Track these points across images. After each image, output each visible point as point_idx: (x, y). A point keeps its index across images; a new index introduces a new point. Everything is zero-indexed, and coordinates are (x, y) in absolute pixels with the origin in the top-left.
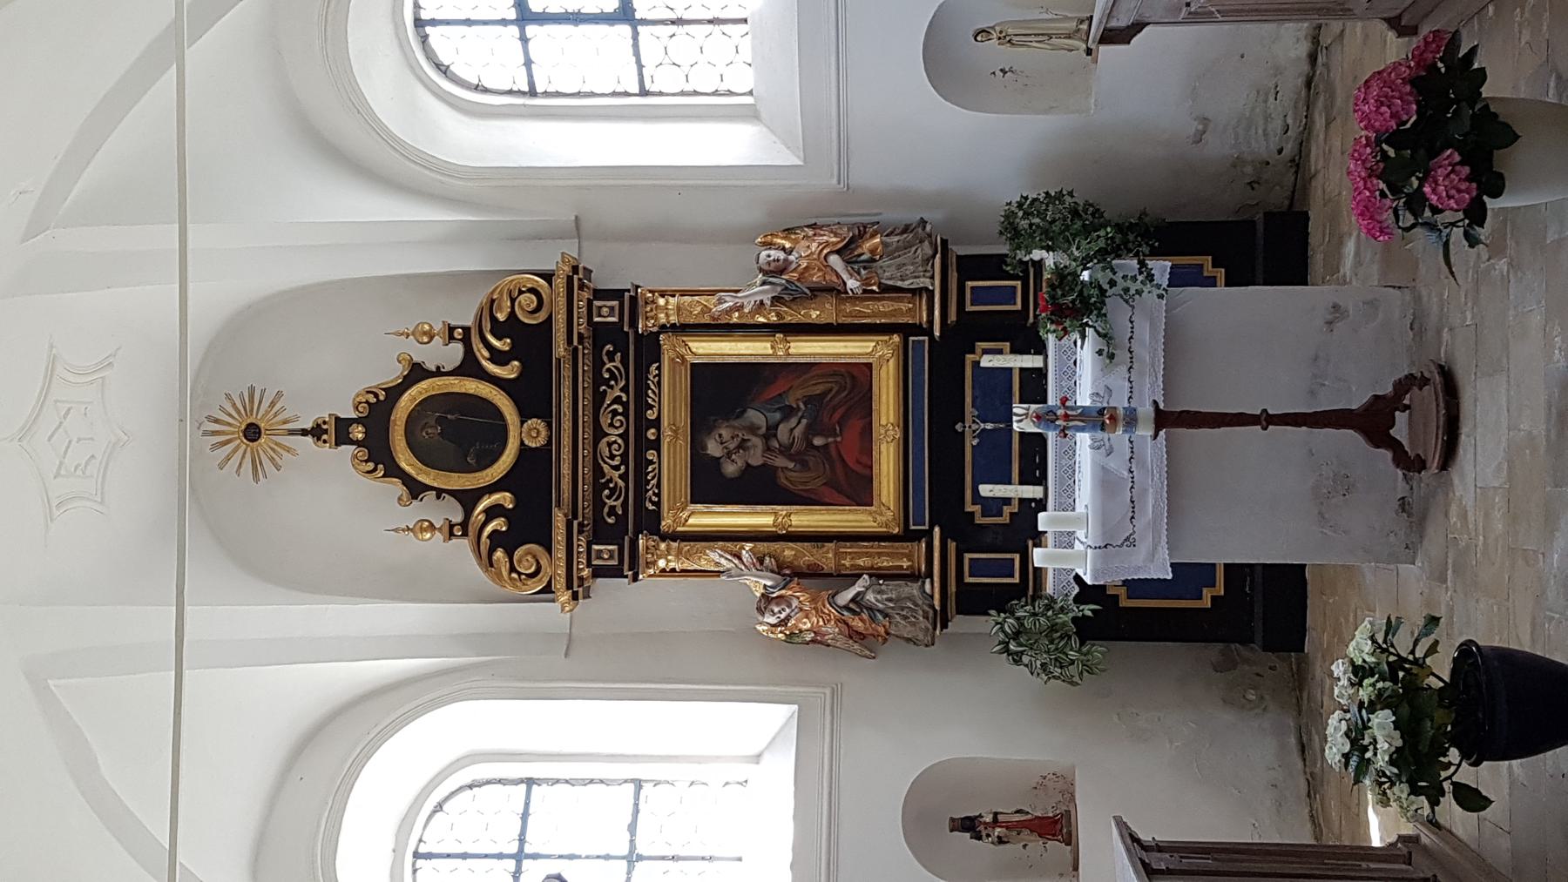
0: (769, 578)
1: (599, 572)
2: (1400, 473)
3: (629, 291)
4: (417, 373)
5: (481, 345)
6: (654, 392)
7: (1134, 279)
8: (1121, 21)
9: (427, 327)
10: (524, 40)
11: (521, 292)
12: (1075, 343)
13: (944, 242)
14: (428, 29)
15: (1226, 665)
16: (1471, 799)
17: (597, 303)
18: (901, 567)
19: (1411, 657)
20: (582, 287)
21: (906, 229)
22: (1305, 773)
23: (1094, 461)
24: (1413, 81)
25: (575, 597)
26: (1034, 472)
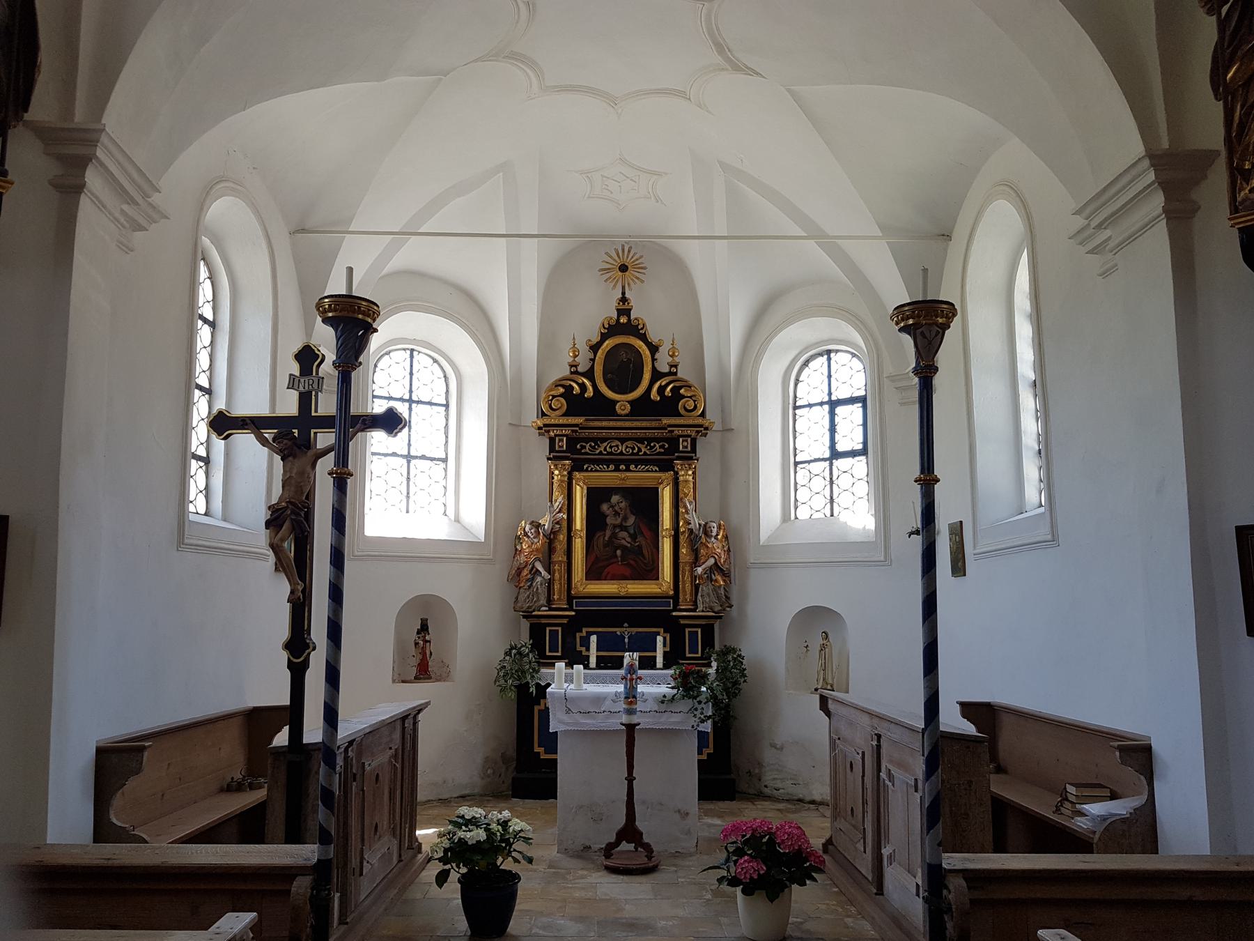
0: (548, 528)
1: (552, 440)
2: (603, 846)
3: (696, 456)
4: (654, 349)
5: (668, 381)
6: (644, 468)
7: (702, 713)
8: (831, 706)
9: (677, 354)
10: (821, 404)
11: (695, 401)
12: (669, 684)
13: (720, 617)
14: (826, 357)
15: (505, 759)
16: (442, 878)
17: (689, 440)
18: (554, 595)
19: (512, 850)
20: (698, 432)
21: (727, 598)
22: (451, 798)
23: (609, 693)
24: (800, 851)
25: (540, 428)
26: (603, 663)
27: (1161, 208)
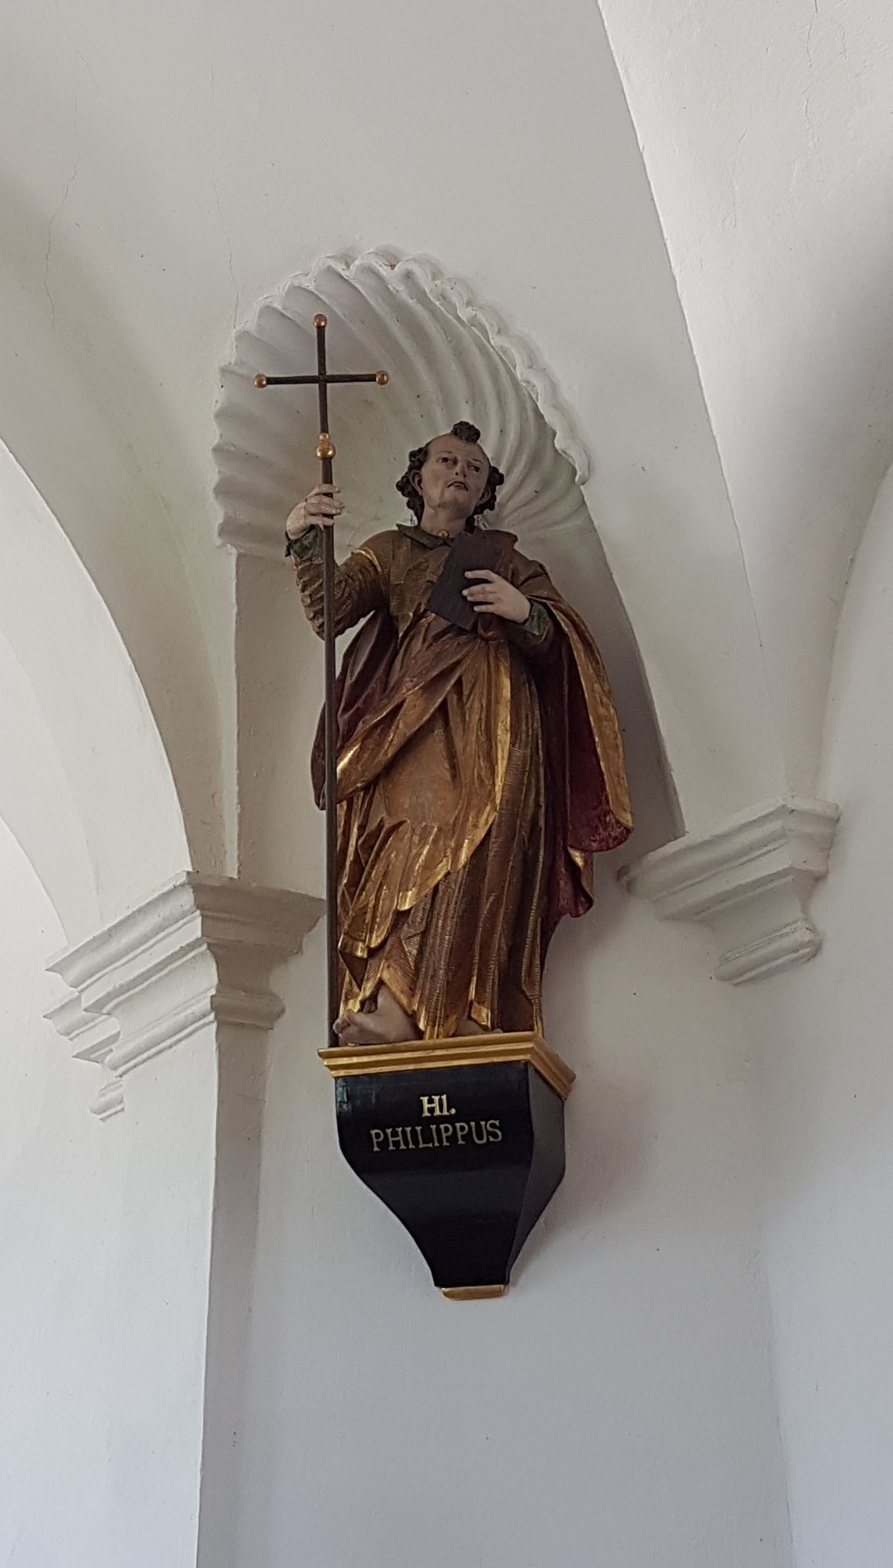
27: (208, 1000)
